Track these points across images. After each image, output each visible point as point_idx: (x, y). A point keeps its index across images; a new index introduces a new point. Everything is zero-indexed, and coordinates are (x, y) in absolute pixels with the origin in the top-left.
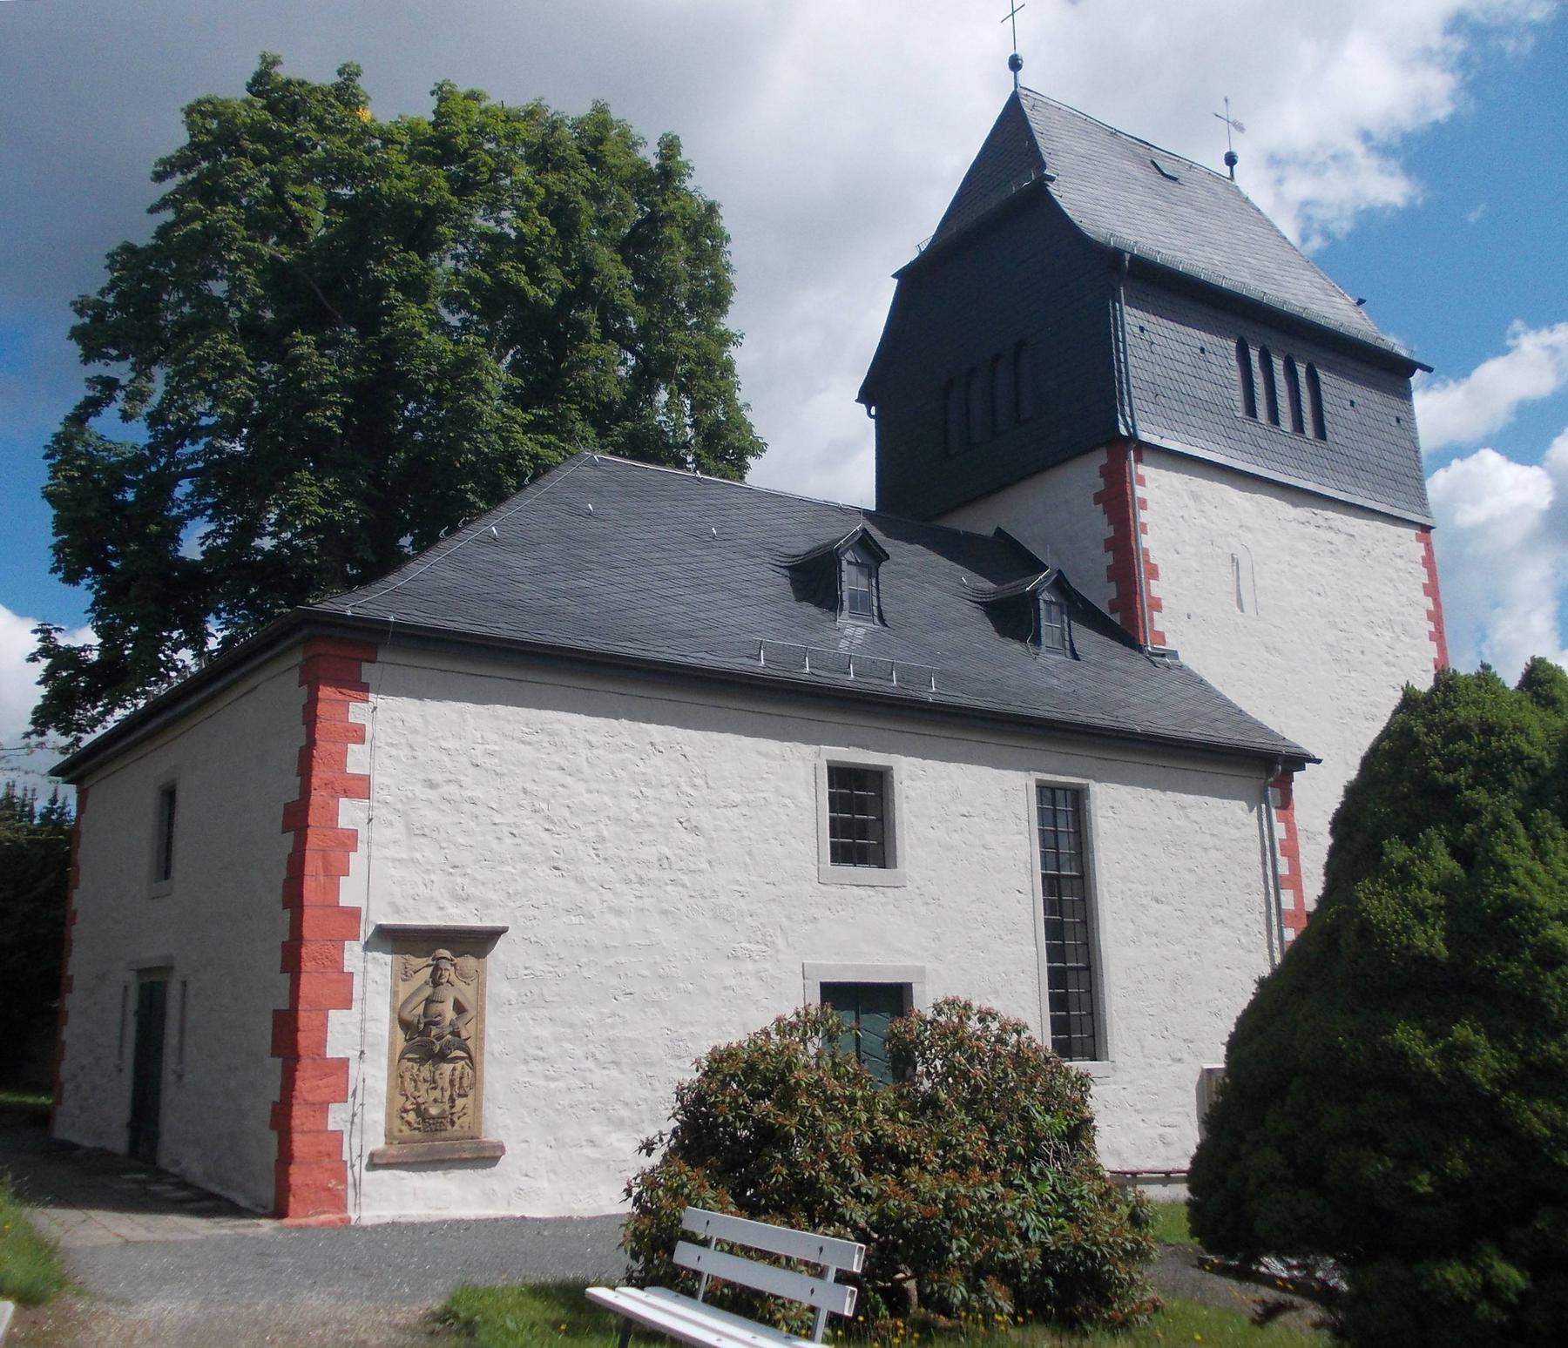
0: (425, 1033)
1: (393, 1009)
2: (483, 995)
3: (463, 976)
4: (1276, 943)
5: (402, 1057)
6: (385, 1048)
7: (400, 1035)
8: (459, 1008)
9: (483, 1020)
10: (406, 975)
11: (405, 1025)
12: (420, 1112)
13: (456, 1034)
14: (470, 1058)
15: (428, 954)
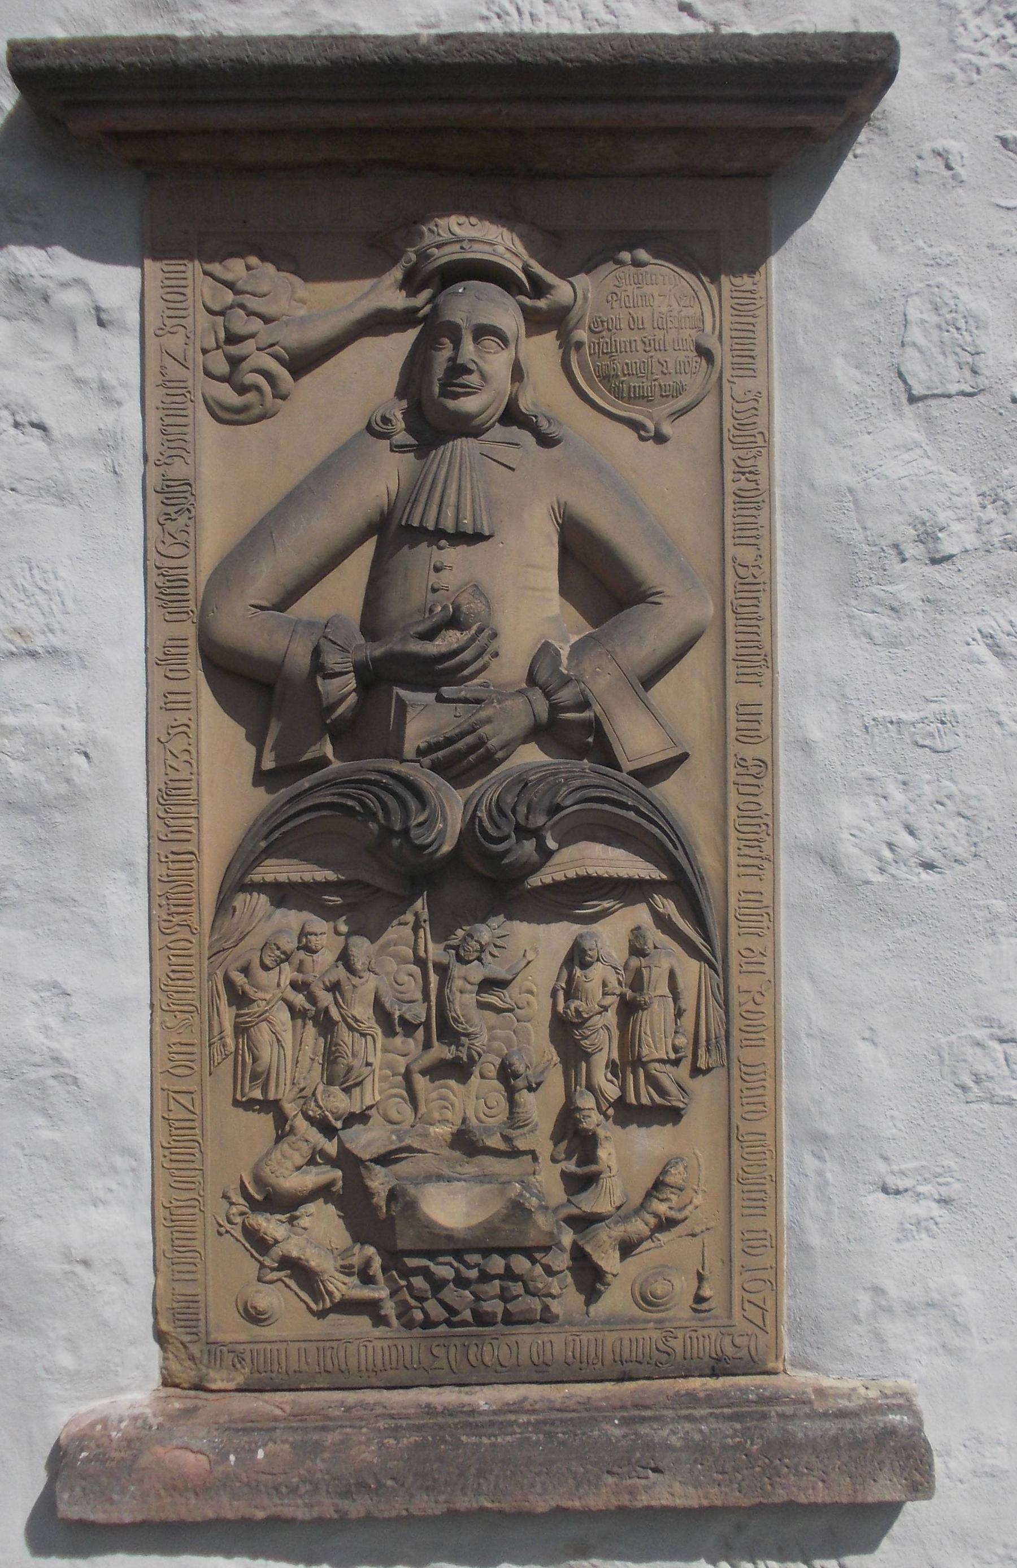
0: (367, 729)
1: (165, 588)
2: (755, 499)
3: (619, 389)
4: (429, 462)
5: (236, 883)
6: (126, 820)
7: (223, 748)
8: (598, 577)
9: (758, 658)
10: (238, 382)
11: (244, 681)
12: (377, 1220)
13: (581, 736)
14: (683, 885)
15: (373, 254)
